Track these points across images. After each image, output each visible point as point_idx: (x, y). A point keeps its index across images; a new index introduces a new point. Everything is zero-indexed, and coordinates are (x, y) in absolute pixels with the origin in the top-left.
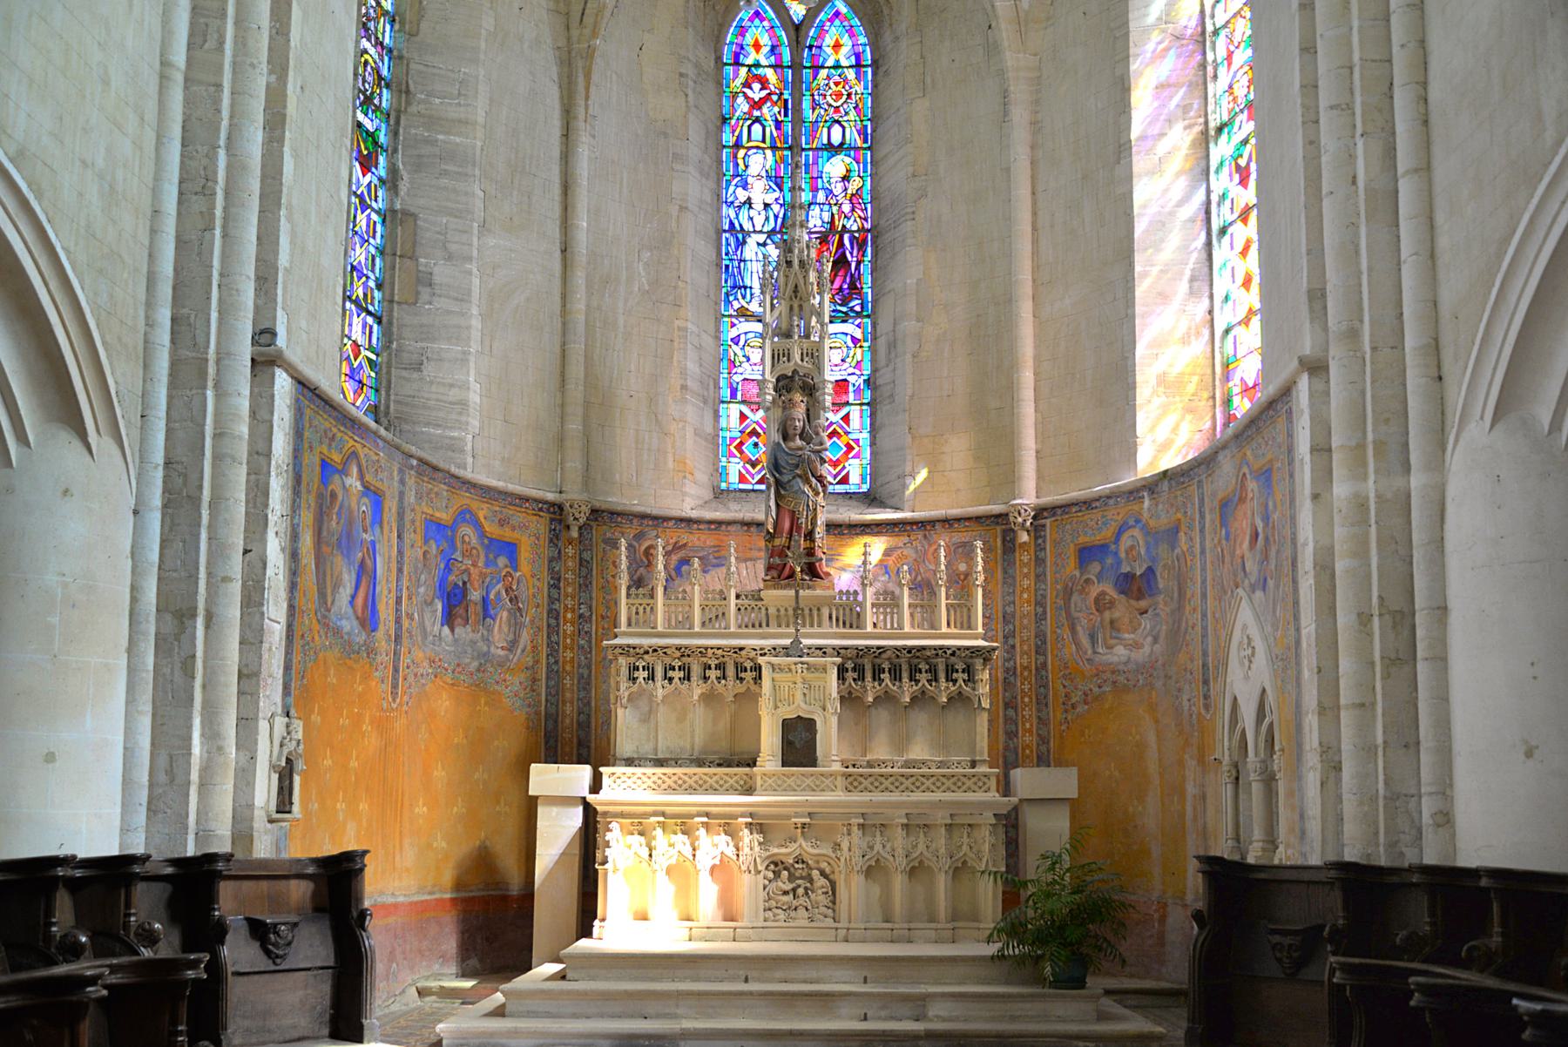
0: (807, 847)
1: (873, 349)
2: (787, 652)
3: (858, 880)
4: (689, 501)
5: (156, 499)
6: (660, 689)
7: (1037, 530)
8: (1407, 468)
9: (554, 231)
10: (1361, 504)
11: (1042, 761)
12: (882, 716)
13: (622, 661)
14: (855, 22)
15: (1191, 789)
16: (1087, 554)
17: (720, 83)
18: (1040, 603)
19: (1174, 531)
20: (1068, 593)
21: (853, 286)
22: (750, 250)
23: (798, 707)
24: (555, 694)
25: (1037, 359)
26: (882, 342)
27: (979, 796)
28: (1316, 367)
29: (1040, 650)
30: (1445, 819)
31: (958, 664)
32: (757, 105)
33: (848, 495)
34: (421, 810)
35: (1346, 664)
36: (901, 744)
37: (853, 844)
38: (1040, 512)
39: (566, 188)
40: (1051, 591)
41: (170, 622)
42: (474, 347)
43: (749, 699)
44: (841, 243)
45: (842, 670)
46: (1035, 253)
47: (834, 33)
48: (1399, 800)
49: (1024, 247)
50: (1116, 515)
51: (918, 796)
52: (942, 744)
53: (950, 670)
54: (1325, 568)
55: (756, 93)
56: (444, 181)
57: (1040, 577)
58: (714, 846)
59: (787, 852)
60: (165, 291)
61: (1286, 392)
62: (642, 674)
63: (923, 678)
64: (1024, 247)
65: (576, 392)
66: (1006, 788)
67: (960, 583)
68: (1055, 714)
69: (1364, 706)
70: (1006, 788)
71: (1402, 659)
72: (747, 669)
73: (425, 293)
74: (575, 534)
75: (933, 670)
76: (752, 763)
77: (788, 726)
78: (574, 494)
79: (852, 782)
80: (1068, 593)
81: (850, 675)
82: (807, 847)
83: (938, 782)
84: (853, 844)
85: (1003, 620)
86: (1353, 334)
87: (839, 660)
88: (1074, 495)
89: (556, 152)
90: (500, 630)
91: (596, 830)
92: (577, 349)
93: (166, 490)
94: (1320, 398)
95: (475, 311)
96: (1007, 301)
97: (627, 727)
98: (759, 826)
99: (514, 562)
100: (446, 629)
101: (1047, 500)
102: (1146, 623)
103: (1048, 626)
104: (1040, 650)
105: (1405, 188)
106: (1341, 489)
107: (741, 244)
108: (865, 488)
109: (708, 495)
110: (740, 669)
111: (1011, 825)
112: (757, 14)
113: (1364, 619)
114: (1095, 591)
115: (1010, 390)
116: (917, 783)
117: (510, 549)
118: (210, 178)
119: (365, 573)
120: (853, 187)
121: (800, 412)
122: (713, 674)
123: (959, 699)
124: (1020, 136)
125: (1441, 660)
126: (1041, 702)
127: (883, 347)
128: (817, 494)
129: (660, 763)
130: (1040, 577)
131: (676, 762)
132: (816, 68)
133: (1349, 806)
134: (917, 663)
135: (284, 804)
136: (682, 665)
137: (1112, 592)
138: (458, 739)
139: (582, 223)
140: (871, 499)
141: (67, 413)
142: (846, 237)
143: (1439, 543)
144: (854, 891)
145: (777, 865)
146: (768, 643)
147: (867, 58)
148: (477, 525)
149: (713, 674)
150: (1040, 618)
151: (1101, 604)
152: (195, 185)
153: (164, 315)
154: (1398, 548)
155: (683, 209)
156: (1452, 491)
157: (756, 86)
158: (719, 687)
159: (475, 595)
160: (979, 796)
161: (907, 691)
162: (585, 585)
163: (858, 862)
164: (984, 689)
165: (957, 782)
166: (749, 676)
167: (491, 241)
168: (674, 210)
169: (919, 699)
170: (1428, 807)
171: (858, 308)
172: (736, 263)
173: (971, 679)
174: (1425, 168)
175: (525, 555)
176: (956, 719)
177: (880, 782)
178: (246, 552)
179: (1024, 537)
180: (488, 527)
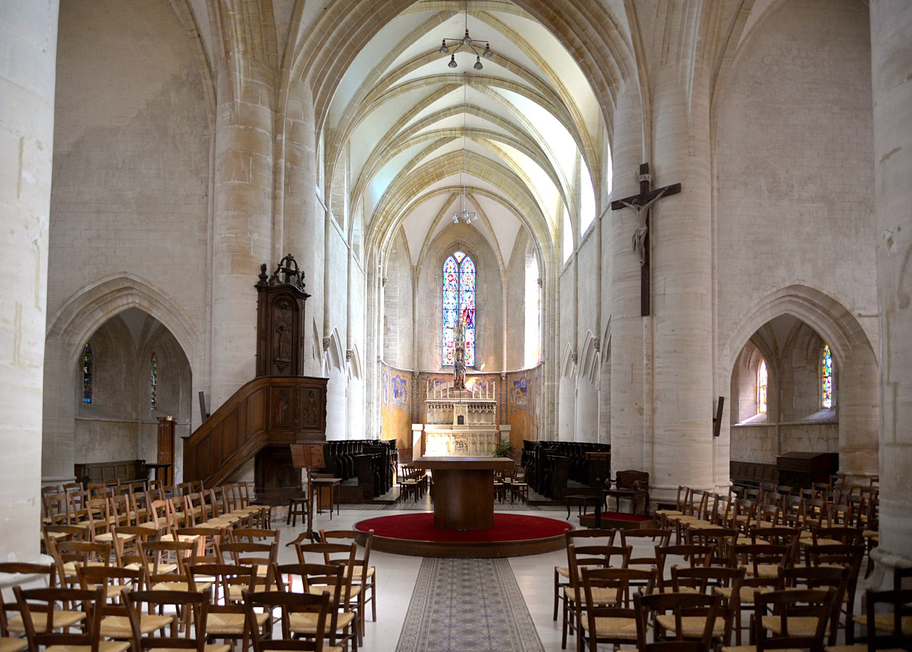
0: (462, 439)
1: (475, 335)
2: (459, 403)
3: (471, 445)
4: (437, 369)
6: (435, 410)
7: (506, 377)
9: (412, 316)
10: (548, 386)
11: (507, 423)
12: (476, 415)
13: (428, 404)
14: (472, 262)
15: (531, 429)
16: (515, 383)
17: (443, 277)
18: (507, 392)
19: (530, 381)
20: (512, 390)
21: (471, 322)
22: (449, 313)
23: (461, 414)
24: (413, 409)
25: (507, 342)
26: (476, 335)
27: (493, 430)
28: (544, 363)
29: (507, 401)
30: (557, 435)
31: (490, 405)
32: (451, 281)
33: (469, 367)
34: (392, 432)
35: (546, 411)
36: (479, 420)
37: (470, 439)
38: (507, 374)
39: (414, 306)
40: (509, 389)
41: (368, 405)
42: (398, 342)
43: (451, 412)
45: (468, 406)
46: (507, 320)
47: (467, 264)
48: (552, 432)
49: (505, 319)
50: (521, 376)
51: (482, 430)
52: (487, 420)
53: (488, 406)
55: (451, 278)
56: (392, 309)
57: (507, 387)
58: (97, 373)
59: (459, 440)
61: (541, 365)
62: (431, 407)
63: (483, 408)
64: (505, 319)
65: (416, 349)
66: (498, 428)
67: (491, 390)
68: (509, 414)
69: (548, 418)
70: (498, 428)
71: (553, 411)
72: (451, 406)
73: (389, 332)
75: (485, 406)
76: (452, 424)
77: (459, 417)
78: (416, 370)
79: (470, 427)
80: (512, 390)
82: (462, 439)
83: (486, 427)
84: (470, 439)
85: (499, 395)
86: (548, 359)
88: (513, 371)
91: (425, 436)
92: (416, 340)
95: (398, 335)
96: (501, 329)
97: (429, 417)
98: (454, 435)
99: (405, 385)
101: (508, 371)
102: (525, 397)
103: (508, 396)
104: (507, 401)
106: (546, 384)
107: (447, 312)
108: (473, 365)
109: (441, 367)
110: (450, 406)
111: (499, 435)
113: (548, 404)
114: (516, 390)
115: (502, 348)
116: (482, 428)
117: (405, 381)
119: (386, 391)
120: (471, 299)
121: (461, 356)
122: (445, 407)
123: (490, 412)
124: (505, 295)
125: (558, 411)
126: (507, 412)
127: (477, 336)
129: (435, 424)
130: (507, 387)
131: (438, 424)
132: (463, 273)
134: (482, 405)
136: (439, 405)
137: (520, 391)
138: (397, 419)
139: (417, 314)
140: (474, 368)
141: (357, 375)
143: (558, 393)
144: (470, 447)
145: (457, 442)
146: (455, 401)
147: (474, 271)
148: (400, 378)
149: (445, 407)
150: (507, 395)
151: (518, 393)
154: (553, 393)
155: (436, 307)
156: (560, 385)
157: (450, 277)
158: (446, 409)
159: (399, 391)
160: (493, 430)
161: (480, 410)
162: (418, 388)
163: (471, 442)
164: (495, 410)
165: (489, 427)
166: (451, 407)
167: (400, 320)
168: (434, 308)
169: (483, 412)
170: (555, 433)
173: (492, 408)
174: (559, 335)
175: (407, 382)
176: (489, 415)
177: (475, 427)
179: (504, 379)
180: (401, 378)
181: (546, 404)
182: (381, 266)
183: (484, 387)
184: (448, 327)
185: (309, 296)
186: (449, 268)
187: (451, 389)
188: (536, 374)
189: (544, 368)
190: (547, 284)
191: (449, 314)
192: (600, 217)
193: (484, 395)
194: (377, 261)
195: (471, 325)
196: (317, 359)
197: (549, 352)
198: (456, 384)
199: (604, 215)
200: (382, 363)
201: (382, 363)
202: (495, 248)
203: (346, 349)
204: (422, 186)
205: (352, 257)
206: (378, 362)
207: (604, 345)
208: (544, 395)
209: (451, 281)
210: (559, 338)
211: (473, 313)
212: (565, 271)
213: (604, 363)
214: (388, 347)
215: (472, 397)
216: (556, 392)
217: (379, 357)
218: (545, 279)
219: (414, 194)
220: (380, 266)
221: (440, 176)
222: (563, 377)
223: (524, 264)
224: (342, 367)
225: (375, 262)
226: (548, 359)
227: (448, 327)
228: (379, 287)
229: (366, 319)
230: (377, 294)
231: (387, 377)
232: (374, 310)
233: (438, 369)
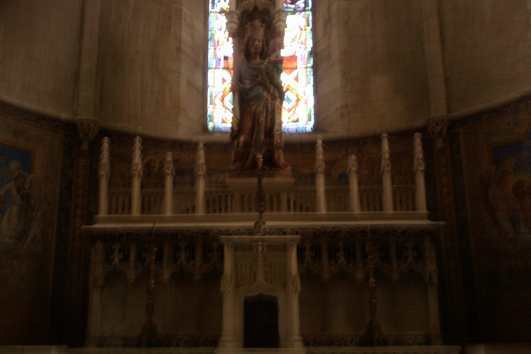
74: (85, 146)
81: (308, 254)
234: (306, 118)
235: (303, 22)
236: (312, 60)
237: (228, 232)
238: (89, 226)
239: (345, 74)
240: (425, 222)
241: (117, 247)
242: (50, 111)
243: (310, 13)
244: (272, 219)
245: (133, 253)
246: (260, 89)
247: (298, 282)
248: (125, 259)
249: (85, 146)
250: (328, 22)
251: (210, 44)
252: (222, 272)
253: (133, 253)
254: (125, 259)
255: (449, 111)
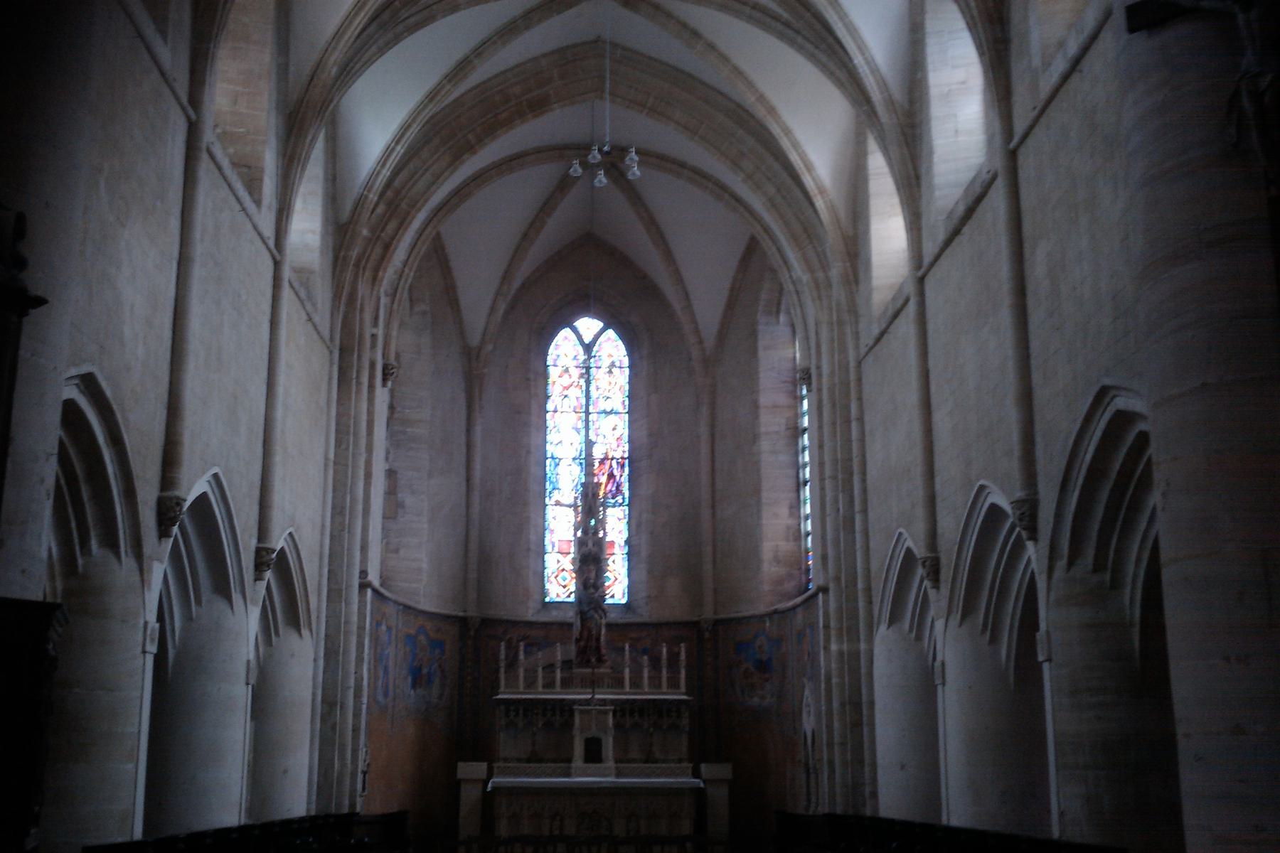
5: (322, 654)
8: (858, 640)
9: (463, 471)
10: (841, 653)
23: (593, 732)
30: (874, 794)
32: (567, 388)
35: (836, 724)
39: (469, 446)
44: (611, 466)
45: (615, 712)
54: (828, 679)
60: (326, 560)
62: (512, 714)
69: (843, 744)
71: (857, 725)
74: (472, 633)
78: (472, 612)
81: (618, 714)
87: (612, 708)
89: (463, 428)
90: (435, 690)
93: (326, 648)
94: (826, 603)
100: (412, 692)
105: (858, 518)
106: (834, 647)
112: (566, 338)
113: (843, 705)
118: (343, 508)
120: (617, 434)
121: (593, 575)
128: (601, 618)
133: (838, 790)
135: (364, 789)
142: (614, 463)
152: (338, 510)
153: (326, 571)
154: (855, 671)
156: (877, 651)
159: (425, 671)
170: (868, 790)
171: (621, 501)
172: (554, 476)
174: (865, 511)
178: (356, 673)
181: (836, 705)
182: (380, 332)
183: (655, 663)
184: (558, 503)
185: (41, 302)
186: (562, 357)
187: (567, 664)
188: (800, 617)
189: (826, 603)
190: (825, 380)
191: (559, 469)
192: (1012, 145)
193: (655, 684)
194: (368, 317)
195: (619, 499)
196: (128, 562)
197: (838, 559)
198: (582, 652)
199: (1026, 135)
200: (375, 591)
201: (375, 591)
202: (677, 305)
203: (254, 542)
204: (492, 128)
205: (286, 285)
206: (364, 586)
207: (1058, 516)
208: (828, 679)
209: (567, 388)
210: (865, 521)
211: (623, 466)
212: (878, 340)
213: (1059, 573)
214: (397, 551)
215: (660, 686)
216: (863, 671)
217: (364, 573)
218: (819, 368)
219: (471, 149)
220: (374, 331)
221: (538, 106)
222: (882, 631)
223: (755, 342)
224: (236, 597)
225: (361, 320)
226: (838, 579)
227: (558, 503)
228: (371, 387)
229: (331, 472)
230: (364, 406)
231: (389, 628)
232: (356, 444)
233: (531, 612)
234: (621, 596)
235: (621, 516)
236: (627, 548)
237: (574, 702)
238: (684, 780)
239: (650, 572)
240: (684, 697)
241: (512, 708)
242: (454, 613)
243: (627, 508)
244: (599, 694)
245: (521, 712)
246: (592, 612)
247: (613, 731)
248: (517, 714)
249: (472, 633)
250: (639, 525)
251: (547, 532)
252: (573, 725)
253: (521, 712)
254: (517, 714)
255: (715, 613)
